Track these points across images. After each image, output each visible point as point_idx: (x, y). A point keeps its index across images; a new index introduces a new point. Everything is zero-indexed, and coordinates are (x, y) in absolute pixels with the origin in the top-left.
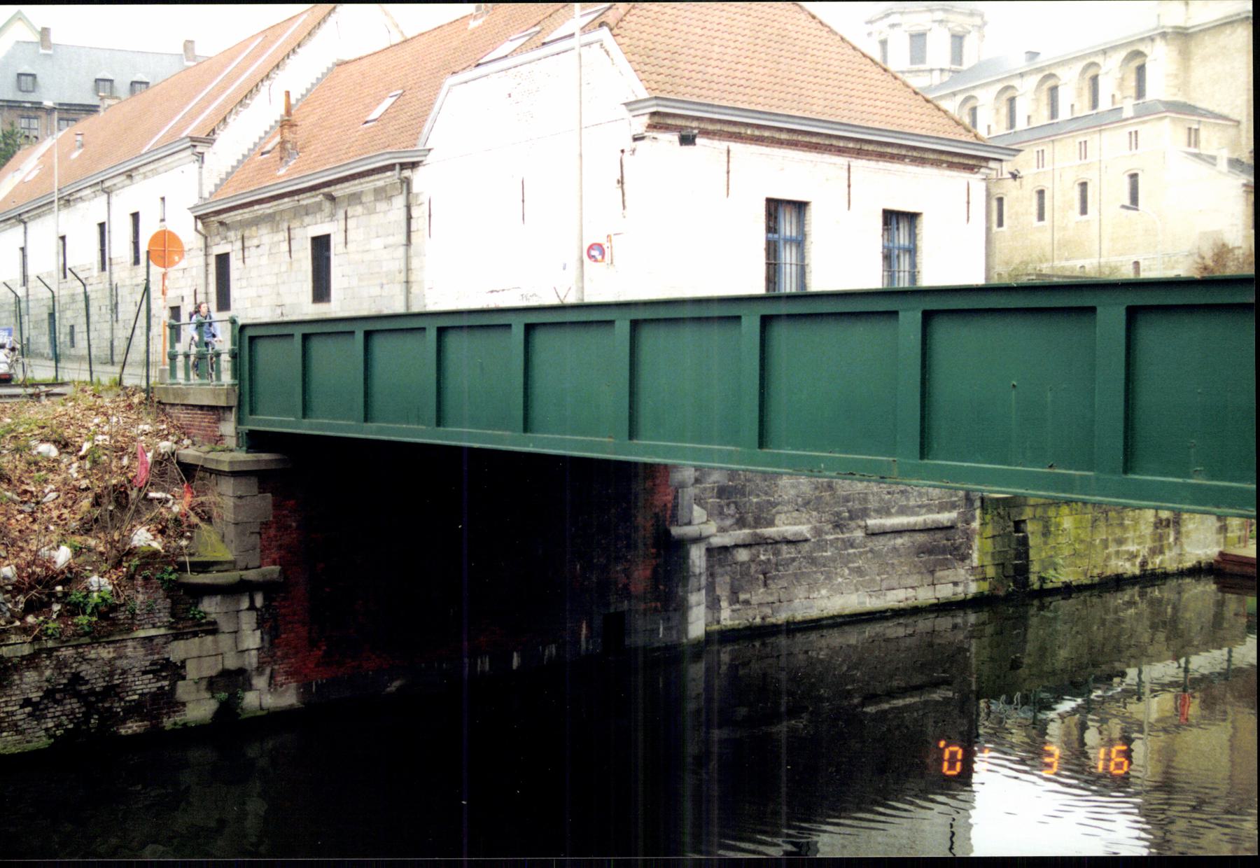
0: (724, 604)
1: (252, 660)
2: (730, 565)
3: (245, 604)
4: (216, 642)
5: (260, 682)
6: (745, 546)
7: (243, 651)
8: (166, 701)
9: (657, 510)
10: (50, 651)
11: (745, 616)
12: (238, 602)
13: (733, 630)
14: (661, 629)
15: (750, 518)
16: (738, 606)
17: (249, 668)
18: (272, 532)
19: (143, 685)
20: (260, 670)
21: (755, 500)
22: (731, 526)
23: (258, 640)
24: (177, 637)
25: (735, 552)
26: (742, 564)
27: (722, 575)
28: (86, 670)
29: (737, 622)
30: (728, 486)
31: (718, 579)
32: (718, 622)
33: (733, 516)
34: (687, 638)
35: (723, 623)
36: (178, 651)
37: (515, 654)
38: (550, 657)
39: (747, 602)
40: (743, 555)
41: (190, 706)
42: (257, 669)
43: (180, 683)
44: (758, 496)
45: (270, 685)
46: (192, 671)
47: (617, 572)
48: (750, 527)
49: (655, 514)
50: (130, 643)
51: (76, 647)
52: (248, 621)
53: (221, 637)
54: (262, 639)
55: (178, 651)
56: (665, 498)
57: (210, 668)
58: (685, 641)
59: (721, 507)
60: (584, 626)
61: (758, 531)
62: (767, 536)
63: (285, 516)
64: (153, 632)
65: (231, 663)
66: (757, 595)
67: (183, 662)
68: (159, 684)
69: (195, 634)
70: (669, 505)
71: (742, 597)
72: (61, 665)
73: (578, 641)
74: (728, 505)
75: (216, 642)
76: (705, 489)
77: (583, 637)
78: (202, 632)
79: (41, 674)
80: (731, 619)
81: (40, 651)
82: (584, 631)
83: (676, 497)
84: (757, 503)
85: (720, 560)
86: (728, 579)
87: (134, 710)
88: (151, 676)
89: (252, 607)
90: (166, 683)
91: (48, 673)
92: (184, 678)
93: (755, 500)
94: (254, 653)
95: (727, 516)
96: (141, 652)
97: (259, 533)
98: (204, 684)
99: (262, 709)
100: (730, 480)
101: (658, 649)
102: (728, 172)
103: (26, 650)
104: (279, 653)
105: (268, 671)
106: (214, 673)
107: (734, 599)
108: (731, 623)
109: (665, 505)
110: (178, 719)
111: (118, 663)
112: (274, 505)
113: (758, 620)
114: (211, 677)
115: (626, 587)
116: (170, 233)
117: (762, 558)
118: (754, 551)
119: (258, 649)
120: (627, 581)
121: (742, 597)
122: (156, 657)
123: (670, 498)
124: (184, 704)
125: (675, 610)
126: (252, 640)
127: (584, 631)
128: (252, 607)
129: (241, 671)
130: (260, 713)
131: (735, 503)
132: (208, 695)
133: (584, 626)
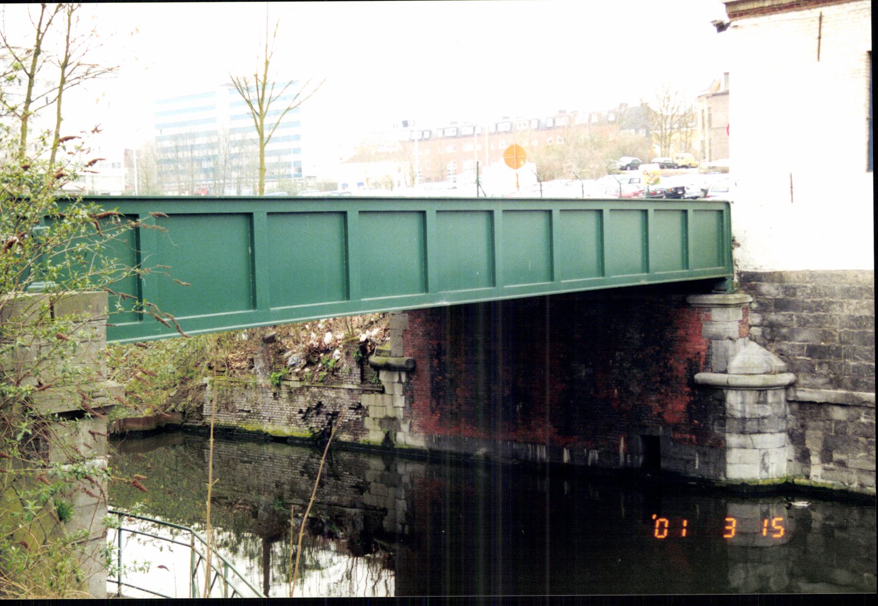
0: (815, 459)
1: (400, 414)
2: (823, 421)
3: (396, 379)
4: (383, 399)
5: (405, 427)
6: (842, 405)
7: (395, 407)
8: (357, 427)
9: (690, 356)
10: (308, 387)
11: (840, 478)
12: (393, 378)
13: (824, 488)
14: (697, 462)
15: (846, 379)
16: (831, 466)
17: (398, 417)
18: (409, 336)
19: (348, 415)
20: (405, 419)
21: (852, 363)
22: (823, 385)
23: (403, 402)
24: (364, 391)
25: (830, 409)
26: (838, 422)
27: (814, 429)
28: (325, 402)
29: (830, 482)
30: (820, 346)
31: (809, 433)
32: (808, 477)
33: (826, 376)
34: (725, 476)
35: (814, 479)
36: (366, 400)
37: (565, 450)
38: (593, 461)
39: (842, 464)
40: (839, 414)
41: (371, 432)
42: (403, 419)
43: (366, 418)
44: (855, 359)
45: (410, 431)
46: (372, 412)
47: (651, 401)
48: (847, 388)
49: (688, 359)
50: (342, 391)
51: (318, 387)
52: (398, 389)
53: (385, 396)
54: (405, 402)
55: (366, 400)
56: (698, 347)
57: (380, 415)
58: (723, 479)
59: (813, 366)
60: (622, 441)
61: (855, 393)
62: (865, 399)
63: (416, 328)
64: (351, 387)
65: (390, 414)
66: (855, 458)
67: (367, 407)
68: (357, 416)
69: (372, 392)
70: (703, 353)
71: (836, 456)
72: (314, 396)
73: (617, 454)
74: (820, 364)
75: (383, 399)
76: (793, 346)
77: (621, 451)
78: (376, 391)
79: (306, 399)
80: (822, 478)
81: (303, 387)
82: (622, 446)
83: (709, 348)
84: (854, 367)
85: (811, 413)
86: (820, 434)
87: (345, 427)
88: (353, 411)
89: (400, 382)
90: (360, 416)
91: (308, 399)
92: (368, 416)
93: (852, 363)
94: (401, 409)
95: (820, 375)
96: (347, 397)
97: (403, 336)
98: (377, 422)
99: (406, 444)
100: (823, 340)
101: (693, 479)
102: (819, 38)
103: (298, 385)
104: (414, 413)
105: (409, 422)
106: (382, 416)
107: (826, 457)
108: (824, 481)
109: (699, 353)
110: (366, 438)
111: (338, 400)
112: (410, 321)
113: (855, 486)
114: (381, 419)
115: (660, 415)
116: (514, 168)
117: (863, 420)
118: (852, 412)
119: (403, 408)
120: (661, 410)
121: (836, 456)
122: (354, 401)
123: (704, 347)
124: (368, 430)
125: (711, 447)
126: (400, 402)
127: (622, 446)
128: (400, 382)
129: (394, 419)
130: (405, 447)
131: (828, 363)
132: (378, 428)
133: (622, 441)
